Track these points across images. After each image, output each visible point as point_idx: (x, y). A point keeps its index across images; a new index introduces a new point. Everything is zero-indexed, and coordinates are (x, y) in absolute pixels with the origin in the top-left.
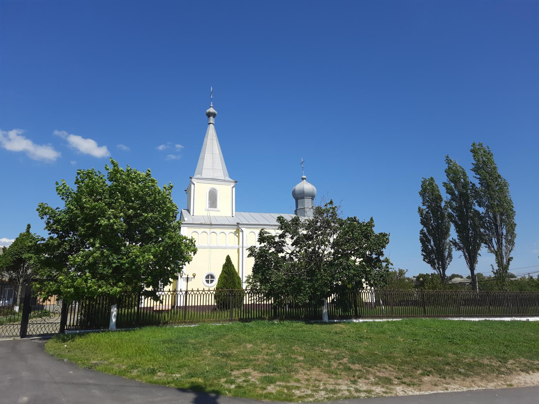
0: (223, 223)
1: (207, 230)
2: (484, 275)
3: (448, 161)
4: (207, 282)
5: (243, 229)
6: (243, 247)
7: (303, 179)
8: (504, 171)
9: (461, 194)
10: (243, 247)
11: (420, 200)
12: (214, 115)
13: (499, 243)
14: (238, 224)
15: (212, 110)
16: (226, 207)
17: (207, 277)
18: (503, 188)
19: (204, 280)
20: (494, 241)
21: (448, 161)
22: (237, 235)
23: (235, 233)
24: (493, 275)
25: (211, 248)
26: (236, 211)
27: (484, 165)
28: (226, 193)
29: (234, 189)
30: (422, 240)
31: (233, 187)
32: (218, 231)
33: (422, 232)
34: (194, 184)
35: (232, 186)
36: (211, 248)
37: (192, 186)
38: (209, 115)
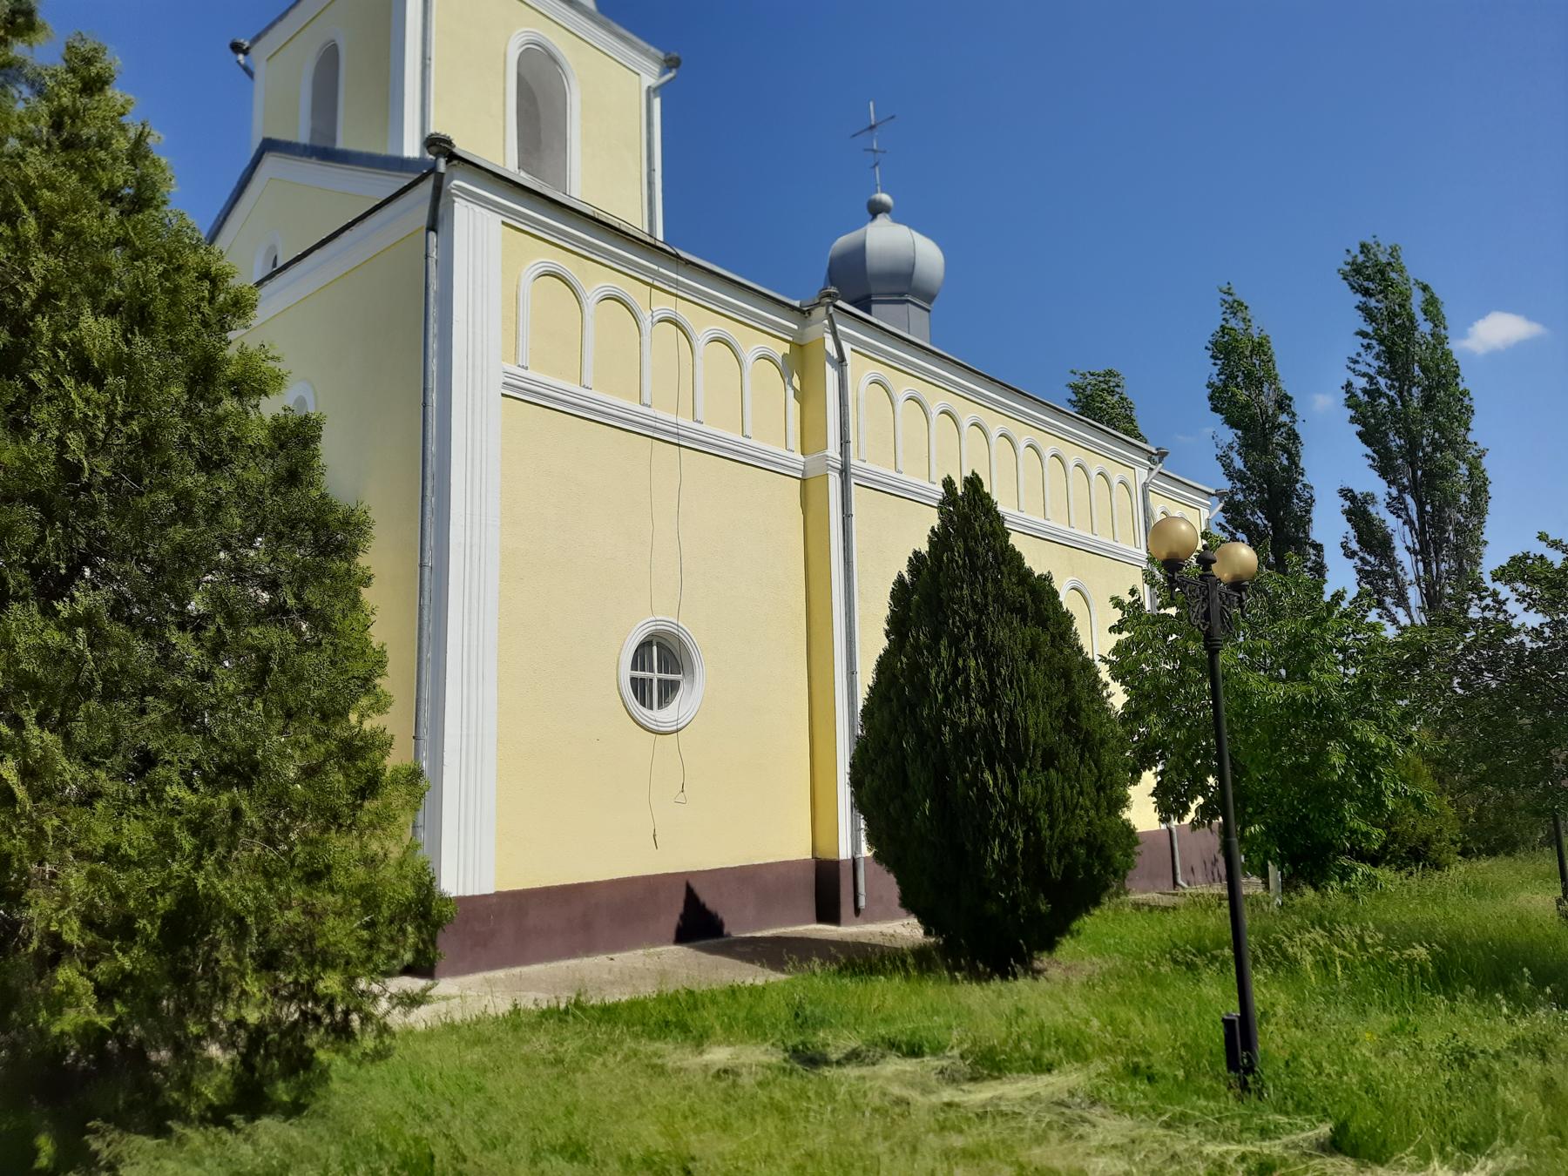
1: (636, 292)
5: (846, 347)
6: (844, 472)
7: (876, 210)
10: (844, 472)
19: (626, 673)
21: (1235, 307)
22: (796, 381)
25: (677, 440)
29: (657, 103)
31: (651, 92)
36: (677, 440)
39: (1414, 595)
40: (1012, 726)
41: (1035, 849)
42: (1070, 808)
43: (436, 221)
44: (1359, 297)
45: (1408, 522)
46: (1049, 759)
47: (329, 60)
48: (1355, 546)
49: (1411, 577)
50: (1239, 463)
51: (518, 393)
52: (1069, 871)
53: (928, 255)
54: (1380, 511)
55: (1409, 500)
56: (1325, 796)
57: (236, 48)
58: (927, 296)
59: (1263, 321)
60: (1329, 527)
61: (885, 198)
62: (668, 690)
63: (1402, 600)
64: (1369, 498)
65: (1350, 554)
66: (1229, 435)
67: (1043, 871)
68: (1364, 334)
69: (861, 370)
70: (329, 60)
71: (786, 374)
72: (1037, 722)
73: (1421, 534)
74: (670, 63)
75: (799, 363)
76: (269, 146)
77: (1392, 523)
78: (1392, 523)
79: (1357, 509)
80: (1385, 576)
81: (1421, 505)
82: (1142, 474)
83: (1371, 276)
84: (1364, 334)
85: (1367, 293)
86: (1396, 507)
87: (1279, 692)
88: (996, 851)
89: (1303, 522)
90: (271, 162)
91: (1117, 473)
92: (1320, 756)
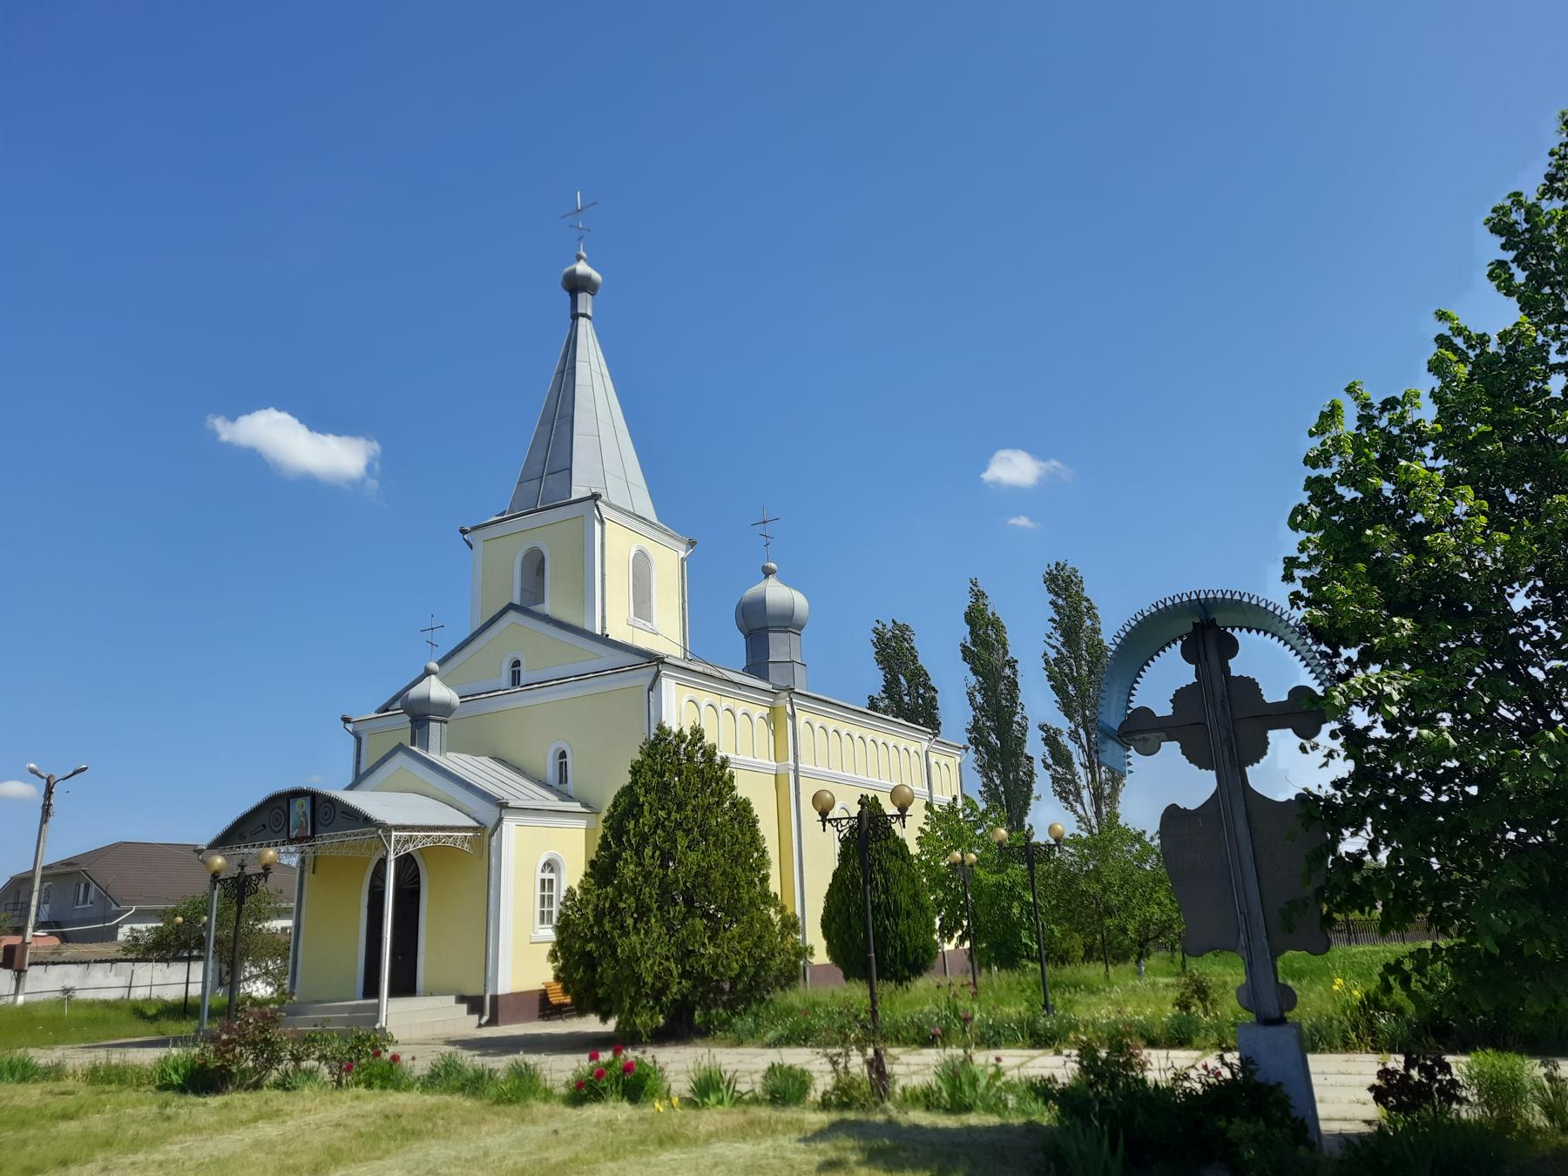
6: (796, 770)
7: (768, 573)
10: (796, 770)
15: (582, 268)
21: (978, 595)
34: (602, 522)
35: (682, 554)
37: (598, 527)
38: (576, 285)
39: (1086, 795)
40: (895, 902)
41: (904, 950)
42: (917, 935)
44: (1052, 597)
45: (1082, 746)
46: (909, 914)
48: (1050, 761)
49: (1084, 783)
50: (979, 699)
52: (916, 959)
53: (800, 602)
54: (1065, 740)
55: (1081, 731)
56: (1014, 928)
57: (463, 532)
59: (996, 606)
60: (1035, 747)
61: (773, 565)
63: (1078, 796)
64: (1058, 732)
65: (1047, 767)
66: (973, 680)
67: (906, 959)
68: (1053, 620)
69: (802, 717)
71: (768, 725)
72: (904, 900)
73: (1089, 756)
74: (692, 544)
75: (773, 718)
76: (511, 607)
77: (1072, 747)
78: (1072, 747)
79: (1051, 739)
80: (1069, 782)
81: (1088, 734)
82: (925, 745)
83: (1062, 584)
84: (1053, 620)
85: (1056, 594)
86: (1074, 736)
87: (993, 879)
88: (890, 952)
89: (1021, 742)
90: (512, 616)
91: (913, 747)
92: (1010, 907)
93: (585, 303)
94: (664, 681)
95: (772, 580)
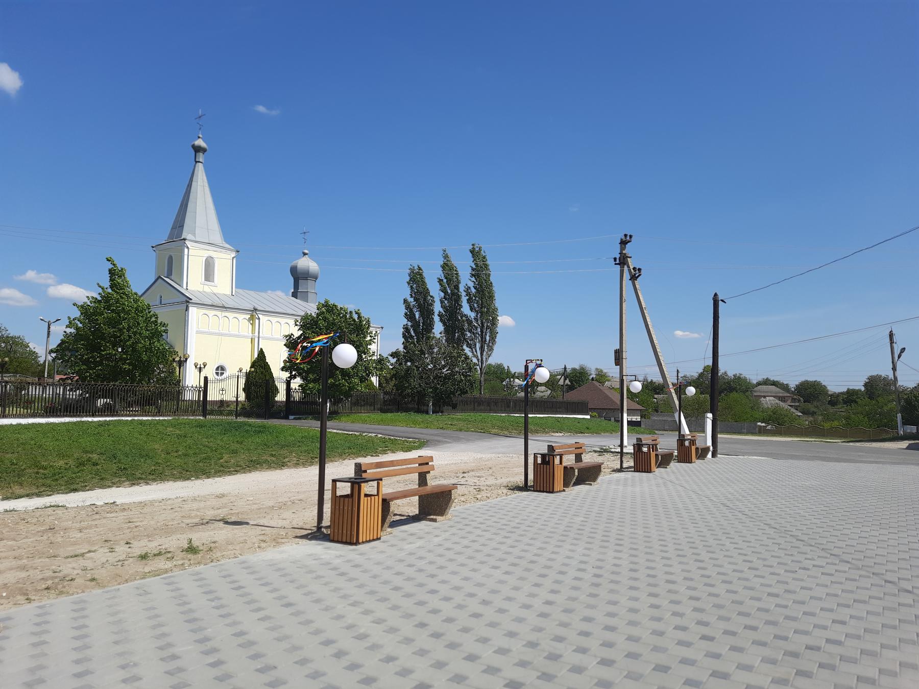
0: (317, 478)
1: (219, 313)
2: (829, 388)
3: (446, 257)
4: (217, 374)
5: (260, 316)
7: (305, 254)
8: (497, 278)
9: (453, 294)
11: (408, 291)
12: (204, 150)
13: (482, 349)
14: (255, 310)
15: (200, 142)
16: (224, 283)
17: (217, 369)
18: (491, 297)
20: (478, 346)
21: (446, 257)
23: (249, 320)
24: (863, 389)
25: (222, 335)
26: (236, 287)
27: (480, 272)
28: (225, 262)
30: (404, 336)
32: (231, 315)
33: (406, 329)
35: (233, 255)
36: (222, 335)
37: (186, 250)
38: (198, 150)
43: (187, 309)
47: (170, 258)
51: (197, 332)
58: (315, 277)
61: (306, 251)
62: (222, 374)
70: (170, 258)
75: (252, 319)
83: (475, 253)
93: (201, 157)
94: (191, 309)
95: (306, 258)
